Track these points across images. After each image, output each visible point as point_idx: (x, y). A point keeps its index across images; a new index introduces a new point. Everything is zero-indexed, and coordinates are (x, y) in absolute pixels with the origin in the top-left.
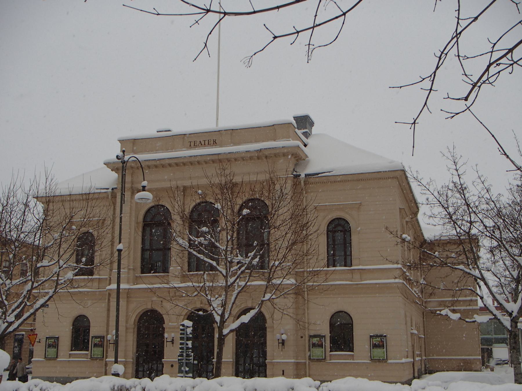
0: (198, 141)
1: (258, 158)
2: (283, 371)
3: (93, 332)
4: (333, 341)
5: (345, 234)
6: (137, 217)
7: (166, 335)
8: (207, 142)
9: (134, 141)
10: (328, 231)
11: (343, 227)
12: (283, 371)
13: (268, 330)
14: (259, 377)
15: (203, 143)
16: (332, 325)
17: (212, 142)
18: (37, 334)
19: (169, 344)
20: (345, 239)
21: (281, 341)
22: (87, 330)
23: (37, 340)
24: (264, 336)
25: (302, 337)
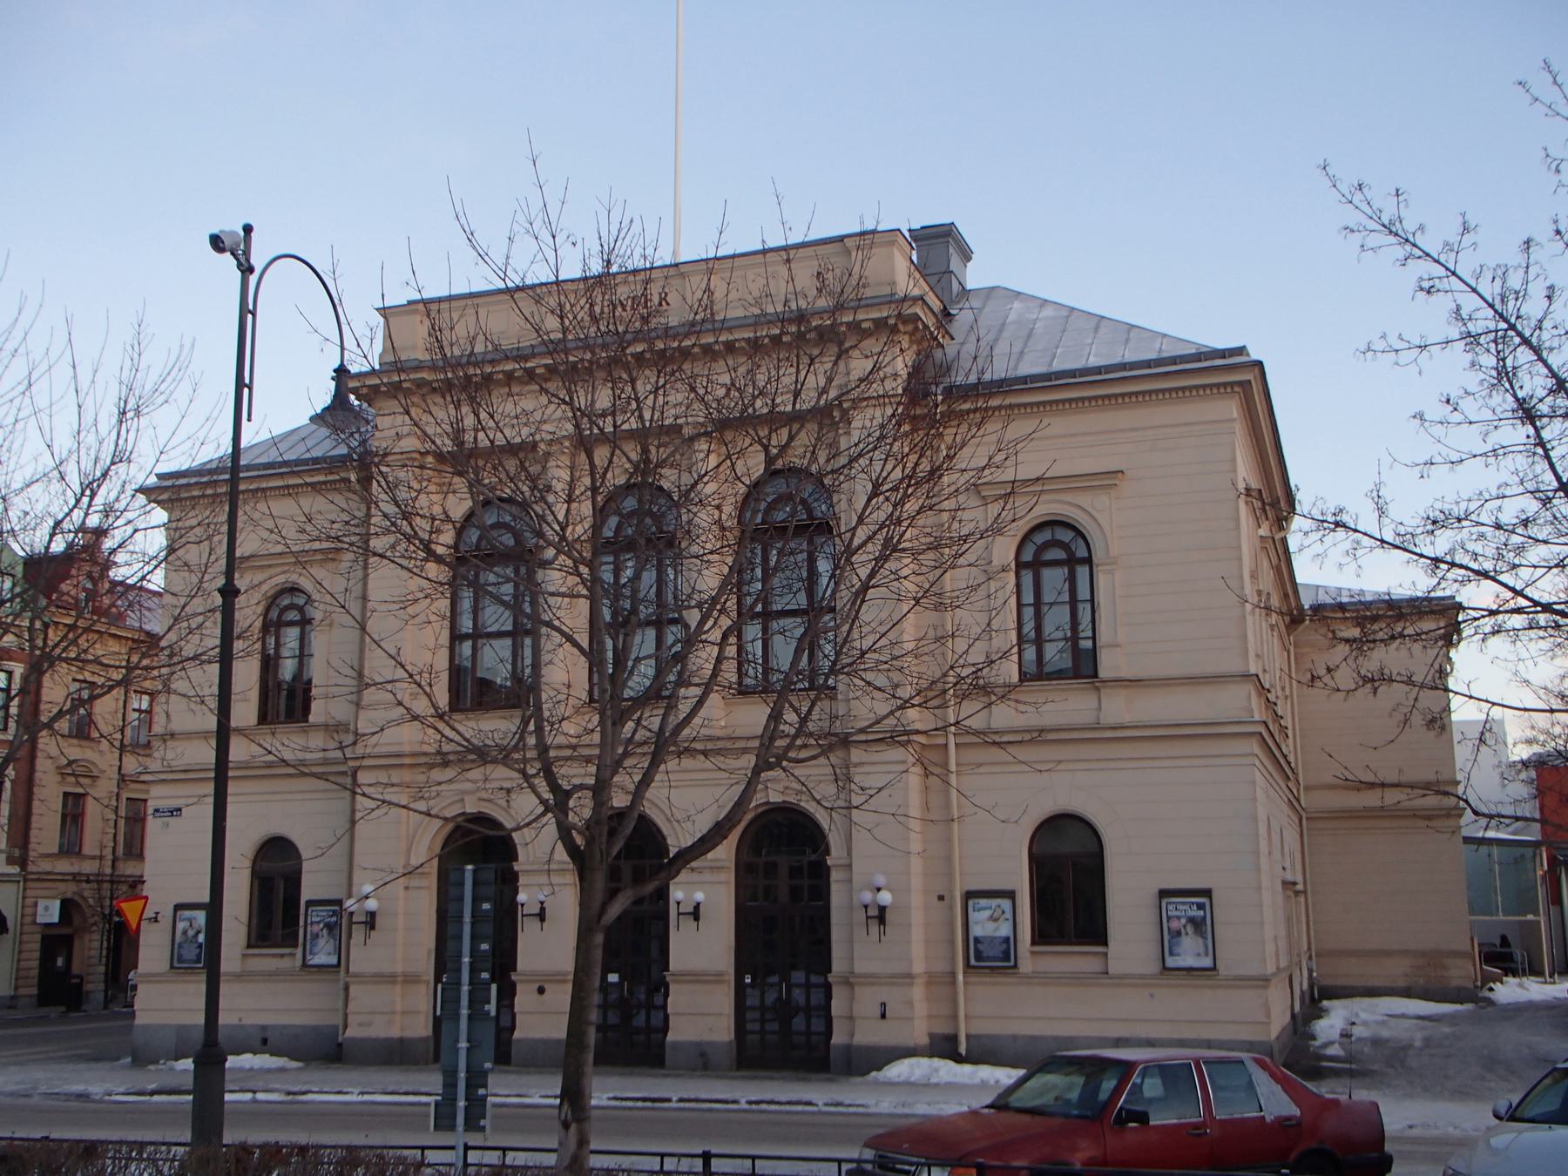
10: (1020, 566)
13: (835, 876)
21: (873, 912)
22: (294, 880)
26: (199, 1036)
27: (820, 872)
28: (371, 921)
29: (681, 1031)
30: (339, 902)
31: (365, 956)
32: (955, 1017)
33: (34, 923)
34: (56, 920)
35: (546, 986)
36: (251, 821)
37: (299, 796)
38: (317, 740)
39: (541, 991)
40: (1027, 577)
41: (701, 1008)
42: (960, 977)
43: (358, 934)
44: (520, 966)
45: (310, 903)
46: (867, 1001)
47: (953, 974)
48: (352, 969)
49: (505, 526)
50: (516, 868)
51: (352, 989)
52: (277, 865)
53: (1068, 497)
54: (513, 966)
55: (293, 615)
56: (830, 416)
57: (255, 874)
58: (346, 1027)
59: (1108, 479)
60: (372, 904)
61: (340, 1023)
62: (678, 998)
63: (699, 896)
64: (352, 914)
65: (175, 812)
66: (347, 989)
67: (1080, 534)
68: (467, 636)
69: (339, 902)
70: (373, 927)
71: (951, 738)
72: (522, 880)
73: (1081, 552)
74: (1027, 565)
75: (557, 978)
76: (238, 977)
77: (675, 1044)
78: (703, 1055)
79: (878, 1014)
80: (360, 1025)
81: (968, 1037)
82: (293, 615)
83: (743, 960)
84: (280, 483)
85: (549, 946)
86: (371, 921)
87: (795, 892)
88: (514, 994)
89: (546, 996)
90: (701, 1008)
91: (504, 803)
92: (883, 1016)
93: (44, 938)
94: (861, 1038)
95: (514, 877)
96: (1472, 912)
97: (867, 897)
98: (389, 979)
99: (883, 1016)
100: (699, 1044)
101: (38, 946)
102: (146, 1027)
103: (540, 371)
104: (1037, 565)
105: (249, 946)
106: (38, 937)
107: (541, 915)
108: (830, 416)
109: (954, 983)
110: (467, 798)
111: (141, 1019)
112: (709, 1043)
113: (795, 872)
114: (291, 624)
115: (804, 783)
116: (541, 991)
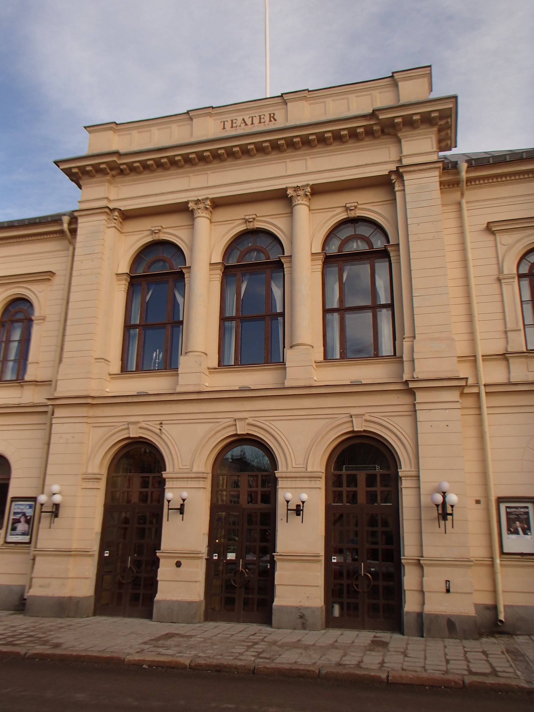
0: (240, 119)
7: (169, 495)
15: (249, 122)
27: (392, 481)
28: (55, 511)
29: (284, 597)
30: (34, 499)
31: (48, 537)
32: (495, 591)
35: (182, 561)
37: (77, 420)
39: (178, 564)
42: (498, 561)
43: (45, 521)
44: (162, 547)
45: (14, 499)
46: (434, 579)
47: (492, 559)
48: (39, 546)
50: (277, 475)
51: (38, 559)
56: (387, 184)
58: (30, 587)
60: (57, 499)
61: (27, 583)
62: (283, 574)
63: (304, 496)
64: (42, 505)
66: (34, 559)
69: (34, 499)
70: (56, 516)
71: (483, 388)
72: (168, 484)
75: (193, 556)
77: (159, 601)
78: (302, 617)
79: (444, 590)
80: (41, 586)
81: (505, 606)
82: (20, 316)
83: (331, 548)
86: (55, 511)
87: (372, 498)
88: (158, 567)
89: (182, 568)
91: (158, 431)
92: (448, 591)
94: (430, 608)
95: (162, 482)
96: (257, 503)
98: (67, 553)
99: (448, 591)
100: (298, 608)
107: (181, 510)
108: (387, 184)
109: (492, 565)
110: (131, 427)
112: (307, 608)
113: (371, 480)
115: (385, 418)
116: (178, 564)
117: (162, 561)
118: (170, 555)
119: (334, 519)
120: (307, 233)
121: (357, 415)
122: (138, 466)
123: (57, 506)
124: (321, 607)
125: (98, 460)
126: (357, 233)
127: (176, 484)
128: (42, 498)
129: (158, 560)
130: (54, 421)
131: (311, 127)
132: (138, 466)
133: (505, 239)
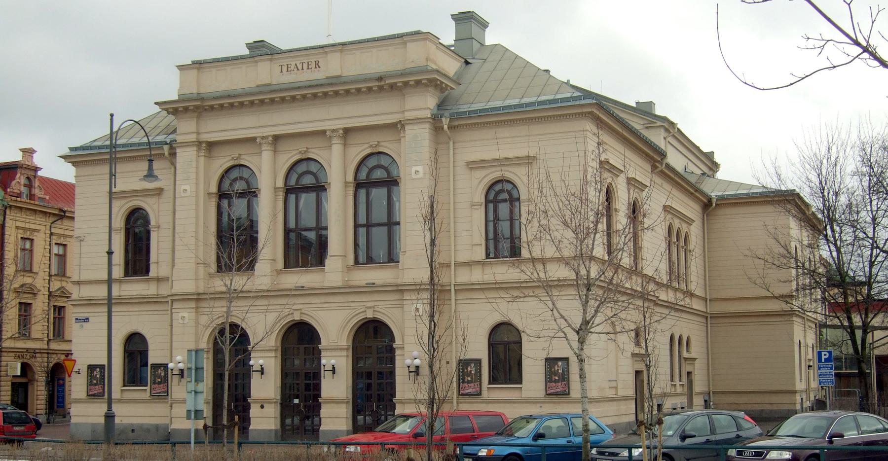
0: (293, 64)
1: (381, 88)
2: (112, 115)
3: (153, 359)
4: (493, 368)
5: (511, 204)
6: (207, 183)
7: (323, 361)
8: (305, 66)
9: (199, 65)
10: (487, 202)
11: (509, 192)
12: (112, 115)
13: (397, 352)
14: (326, 228)
15: (300, 67)
16: (492, 346)
17: (313, 66)
18: (75, 361)
19: (176, 379)
20: (511, 212)
21: (412, 369)
22: (144, 354)
23: (76, 369)
24: (392, 360)
25: (448, 363)
26: (101, 429)
29: (327, 425)
33: (7, 375)
34: (19, 374)
36: (123, 327)
38: (528, 268)
39: (262, 407)
40: (491, 206)
41: (264, 418)
44: (322, 396)
49: (235, 180)
52: (136, 347)
53: (509, 168)
54: (319, 395)
55: (505, 196)
56: (397, 127)
57: (126, 351)
59: (529, 160)
65: (86, 320)
67: (515, 186)
68: (362, 226)
72: (323, 354)
73: (515, 195)
74: (491, 202)
75: (269, 401)
76: (120, 401)
77: (324, 431)
82: (505, 196)
84: (580, 111)
85: (266, 387)
90: (264, 418)
93: (13, 384)
97: (408, 362)
101: (9, 388)
102: (76, 424)
103: (375, 88)
104: (496, 202)
105: (124, 386)
106: (9, 383)
111: (74, 420)
114: (504, 201)
116: (262, 407)
117: (323, 405)
118: (257, 401)
119: (357, 374)
120: (338, 167)
121: (370, 307)
122: (233, 343)
123: (417, 367)
124: (276, 431)
125: (205, 339)
126: (370, 166)
127: (329, 353)
128: (171, 365)
129: (249, 404)
130: (174, 311)
131: (281, 87)
132: (233, 343)
133: (479, 174)
